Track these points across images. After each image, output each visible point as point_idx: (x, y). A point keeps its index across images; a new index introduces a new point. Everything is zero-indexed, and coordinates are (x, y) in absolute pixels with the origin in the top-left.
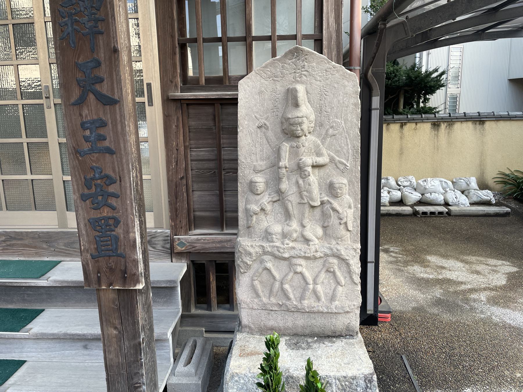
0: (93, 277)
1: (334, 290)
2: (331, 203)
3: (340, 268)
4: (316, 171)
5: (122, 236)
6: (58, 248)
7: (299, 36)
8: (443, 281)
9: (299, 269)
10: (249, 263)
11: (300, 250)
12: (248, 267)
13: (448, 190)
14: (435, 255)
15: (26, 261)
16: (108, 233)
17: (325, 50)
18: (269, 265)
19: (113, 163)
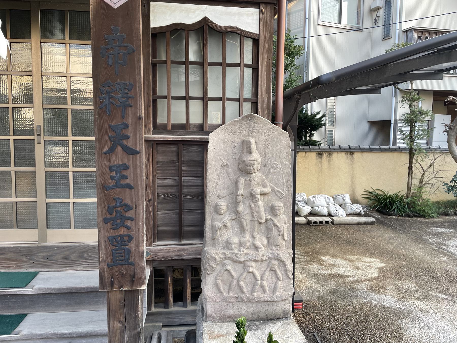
0: (107, 281)
1: (275, 284)
2: (273, 221)
3: (279, 268)
4: (262, 197)
5: (133, 249)
6: (37, 261)
7: (241, 99)
8: (335, 276)
9: (251, 269)
10: (214, 266)
11: (252, 255)
12: (213, 269)
13: (330, 204)
14: (327, 255)
15: (7, 273)
16: (123, 247)
17: (260, 110)
18: (229, 267)
19: (131, 195)
